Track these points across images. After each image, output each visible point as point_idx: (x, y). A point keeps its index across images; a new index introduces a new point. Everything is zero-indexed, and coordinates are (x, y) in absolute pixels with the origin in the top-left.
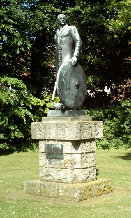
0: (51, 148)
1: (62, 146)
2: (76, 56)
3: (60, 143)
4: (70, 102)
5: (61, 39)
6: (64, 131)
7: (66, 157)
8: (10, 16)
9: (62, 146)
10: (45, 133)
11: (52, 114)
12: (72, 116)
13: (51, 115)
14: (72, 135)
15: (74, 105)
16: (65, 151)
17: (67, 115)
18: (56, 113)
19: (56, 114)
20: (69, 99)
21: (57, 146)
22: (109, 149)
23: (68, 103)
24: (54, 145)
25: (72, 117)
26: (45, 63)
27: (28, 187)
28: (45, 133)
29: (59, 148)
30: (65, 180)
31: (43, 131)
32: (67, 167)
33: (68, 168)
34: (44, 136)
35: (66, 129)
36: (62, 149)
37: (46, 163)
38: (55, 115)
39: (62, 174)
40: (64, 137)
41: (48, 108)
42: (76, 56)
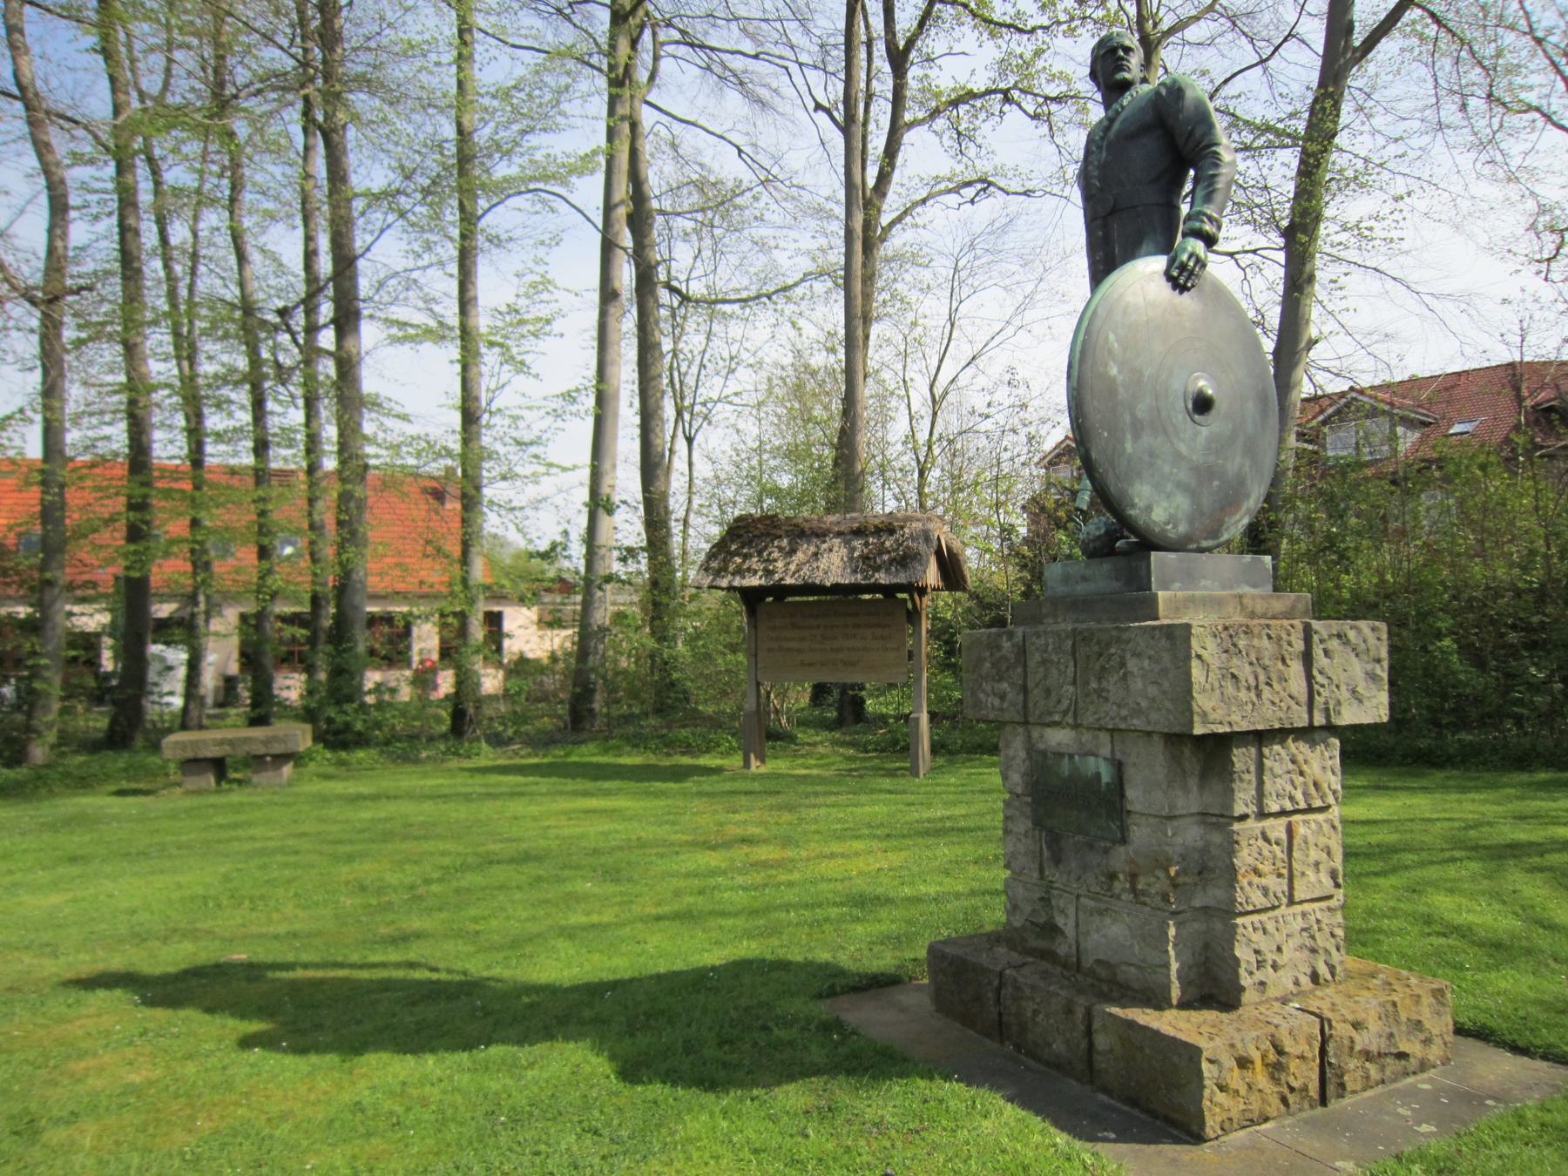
1: (1118, 767)
4: (1165, 504)
5: (581, 666)
7: (1140, 833)
9: (1118, 767)
12: (1181, 589)
13: (1061, 589)
15: (1191, 521)
18: (1088, 572)
19: (1084, 579)
20: (1158, 487)
23: (1149, 509)
24: (1071, 756)
25: (1179, 594)
26: (349, 902)
29: (1098, 775)
30: (1133, 969)
35: (1132, 664)
38: (1081, 588)
41: (964, 590)
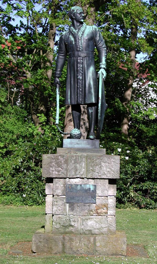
0: (76, 190)
2: (104, 68)
3: (92, 182)
6: (101, 167)
8: (123, 17)
10: (67, 170)
11: (71, 143)
14: (113, 173)
16: (99, 192)
17: (97, 146)
18: (79, 142)
19: (78, 144)
21: (88, 186)
22: (117, 191)
27: (39, 244)
28: (67, 170)
29: (90, 189)
31: (65, 166)
32: (102, 213)
33: (101, 214)
34: (66, 174)
36: (95, 191)
37: (65, 209)
39: (92, 223)
40: (100, 174)
42: (104, 68)
